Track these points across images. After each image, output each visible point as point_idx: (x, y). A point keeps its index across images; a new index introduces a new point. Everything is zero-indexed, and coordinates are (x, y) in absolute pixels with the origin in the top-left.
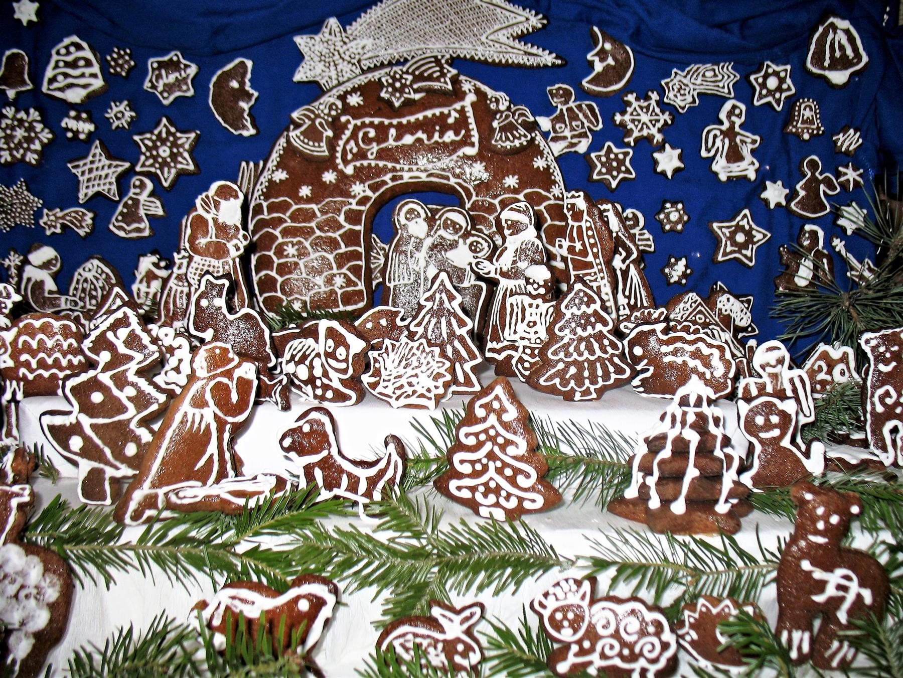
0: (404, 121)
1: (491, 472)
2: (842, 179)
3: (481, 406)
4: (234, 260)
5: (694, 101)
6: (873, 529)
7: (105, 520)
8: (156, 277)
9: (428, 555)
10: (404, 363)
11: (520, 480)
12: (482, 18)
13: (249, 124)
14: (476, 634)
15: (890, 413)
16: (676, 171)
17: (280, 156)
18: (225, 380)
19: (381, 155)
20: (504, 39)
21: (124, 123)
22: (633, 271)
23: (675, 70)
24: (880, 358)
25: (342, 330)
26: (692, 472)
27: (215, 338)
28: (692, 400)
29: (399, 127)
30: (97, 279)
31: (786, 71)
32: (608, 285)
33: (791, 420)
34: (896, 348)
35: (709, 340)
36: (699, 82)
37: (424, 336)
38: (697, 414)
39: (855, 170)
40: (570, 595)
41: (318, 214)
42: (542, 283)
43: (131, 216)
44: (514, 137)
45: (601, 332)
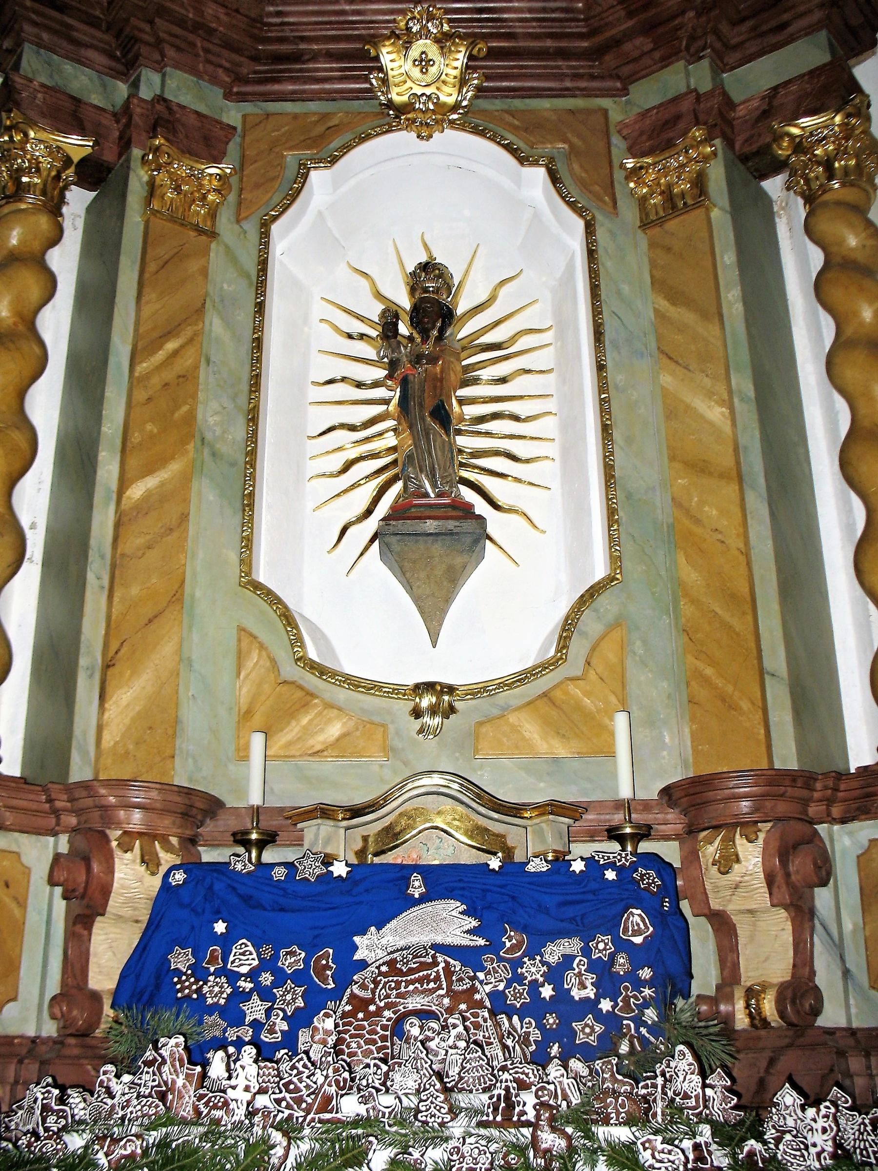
0: (409, 978)
1: (432, 1109)
11: (443, 1111)
13: (331, 982)
16: (551, 997)
20: (459, 934)
22: (517, 1047)
26: (503, 1105)
29: (406, 981)
43: (272, 1031)
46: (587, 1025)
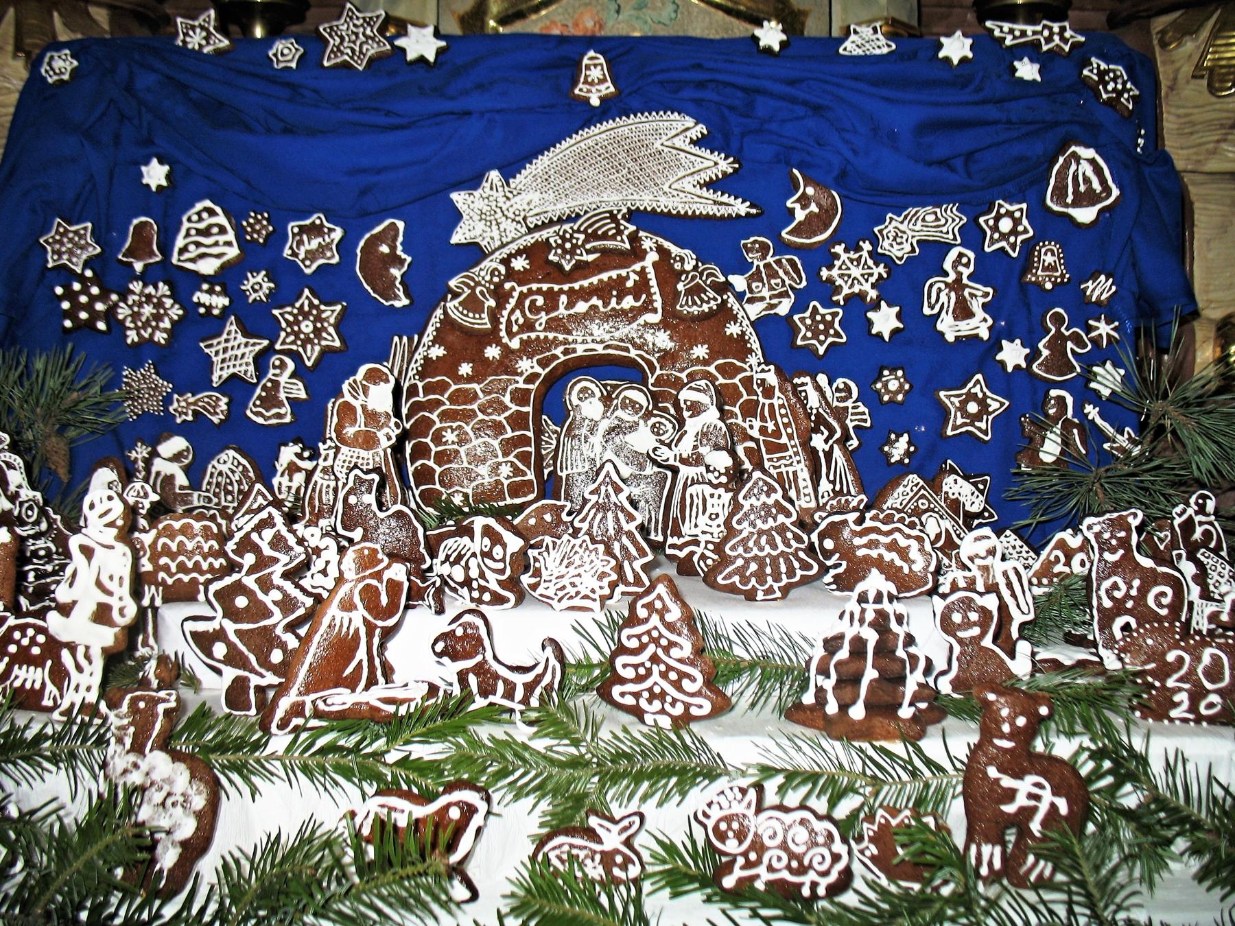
0: (576, 286)
1: (656, 676)
7: (251, 729)
8: (299, 469)
9: (589, 763)
11: (686, 683)
13: (401, 294)
14: (636, 846)
16: (895, 332)
20: (689, 188)
22: (837, 453)
25: (499, 528)
26: (871, 674)
27: (365, 538)
28: (871, 597)
35: (907, 530)
36: (918, 227)
37: (589, 533)
39: (1108, 323)
40: (734, 804)
41: (481, 394)
43: (270, 400)
44: (702, 301)
46: (971, 397)
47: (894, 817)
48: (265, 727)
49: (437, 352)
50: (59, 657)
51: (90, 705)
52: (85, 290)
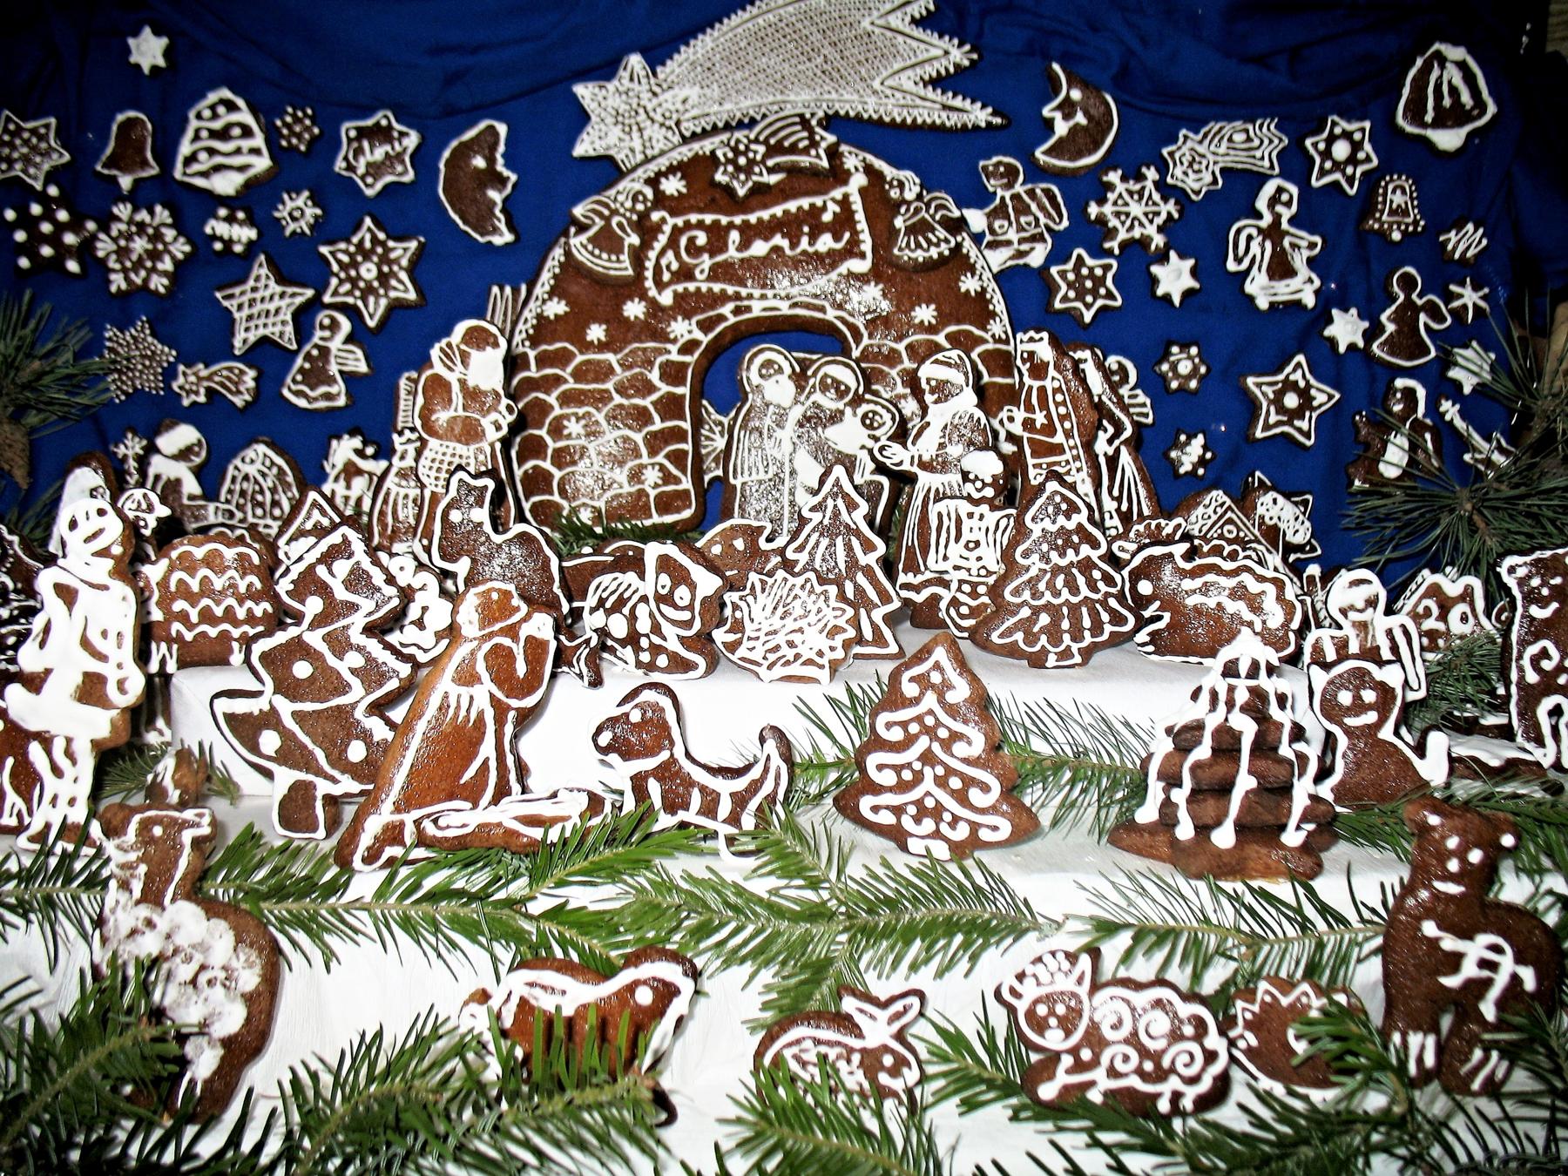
0: (752, 218)
1: (928, 784)
2: (1456, 304)
3: (912, 680)
4: (492, 446)
5: (1215, 181)
6: (1535, 871)
8: (360, 472)
9: (832, 916)
10: (780, 610)
11: (975, 795)
12: (873, 51)
13: (502, 226)
14: (910, 1039)
15: (1549, 685)
16: (1188, 294)
17: (555, 277)
18: (507, 642)
19: (714, 275)
21: (303, 226)
22: (1125, 458)
23: (1184, 132)
24: (1532, 597)
26: (1245, 783)
28: (1243, 668)
30: (264, 475)
31: (1363, 130)
32: (1088, 481)
33: (1394, 698)
34: (1558, 581)
35: (1259, 570)
36: (1222, 150)
37: (809, 566)
38: (1252, 690)
39: (1476, 288)
42: (989, 480)
43: (316, 375)
44: (929, 242)
45: (1088, 558)
46: (1290, 386)
47: (1285, 993)
48: (343, 857)
49: (556, 308)
50: (25, 754)
51: (76, 826)
52: (48, 215)
